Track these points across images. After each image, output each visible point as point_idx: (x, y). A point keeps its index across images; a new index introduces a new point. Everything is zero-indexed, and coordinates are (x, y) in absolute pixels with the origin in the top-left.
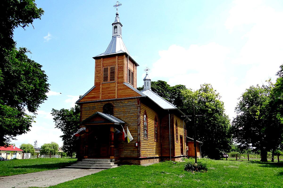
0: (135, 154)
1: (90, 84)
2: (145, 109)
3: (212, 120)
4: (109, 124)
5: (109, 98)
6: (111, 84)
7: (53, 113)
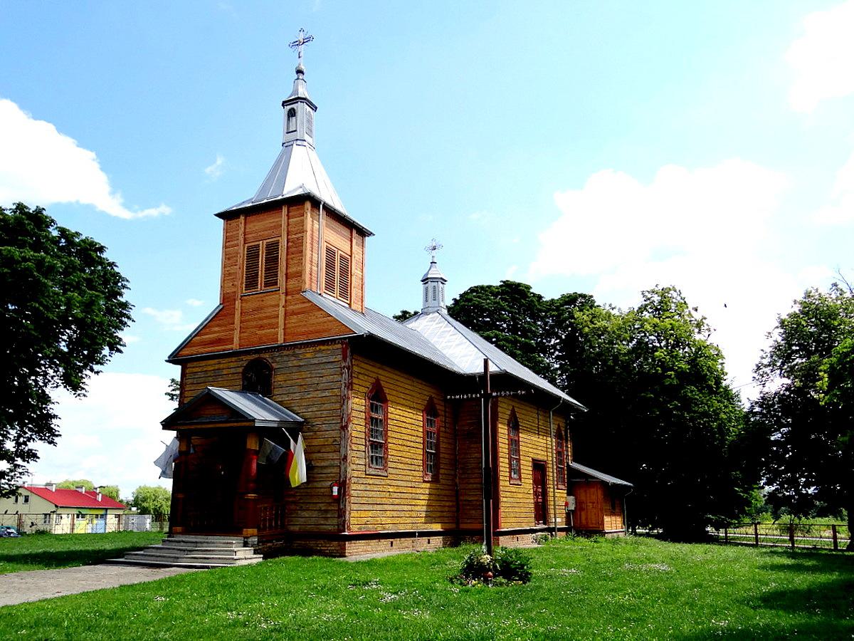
0: (330, 522)
1: (207, 302)
2: (375, 375)
3: (676, 408)
4: (239, 424)
5: (261, 342)
6: (267, 298)
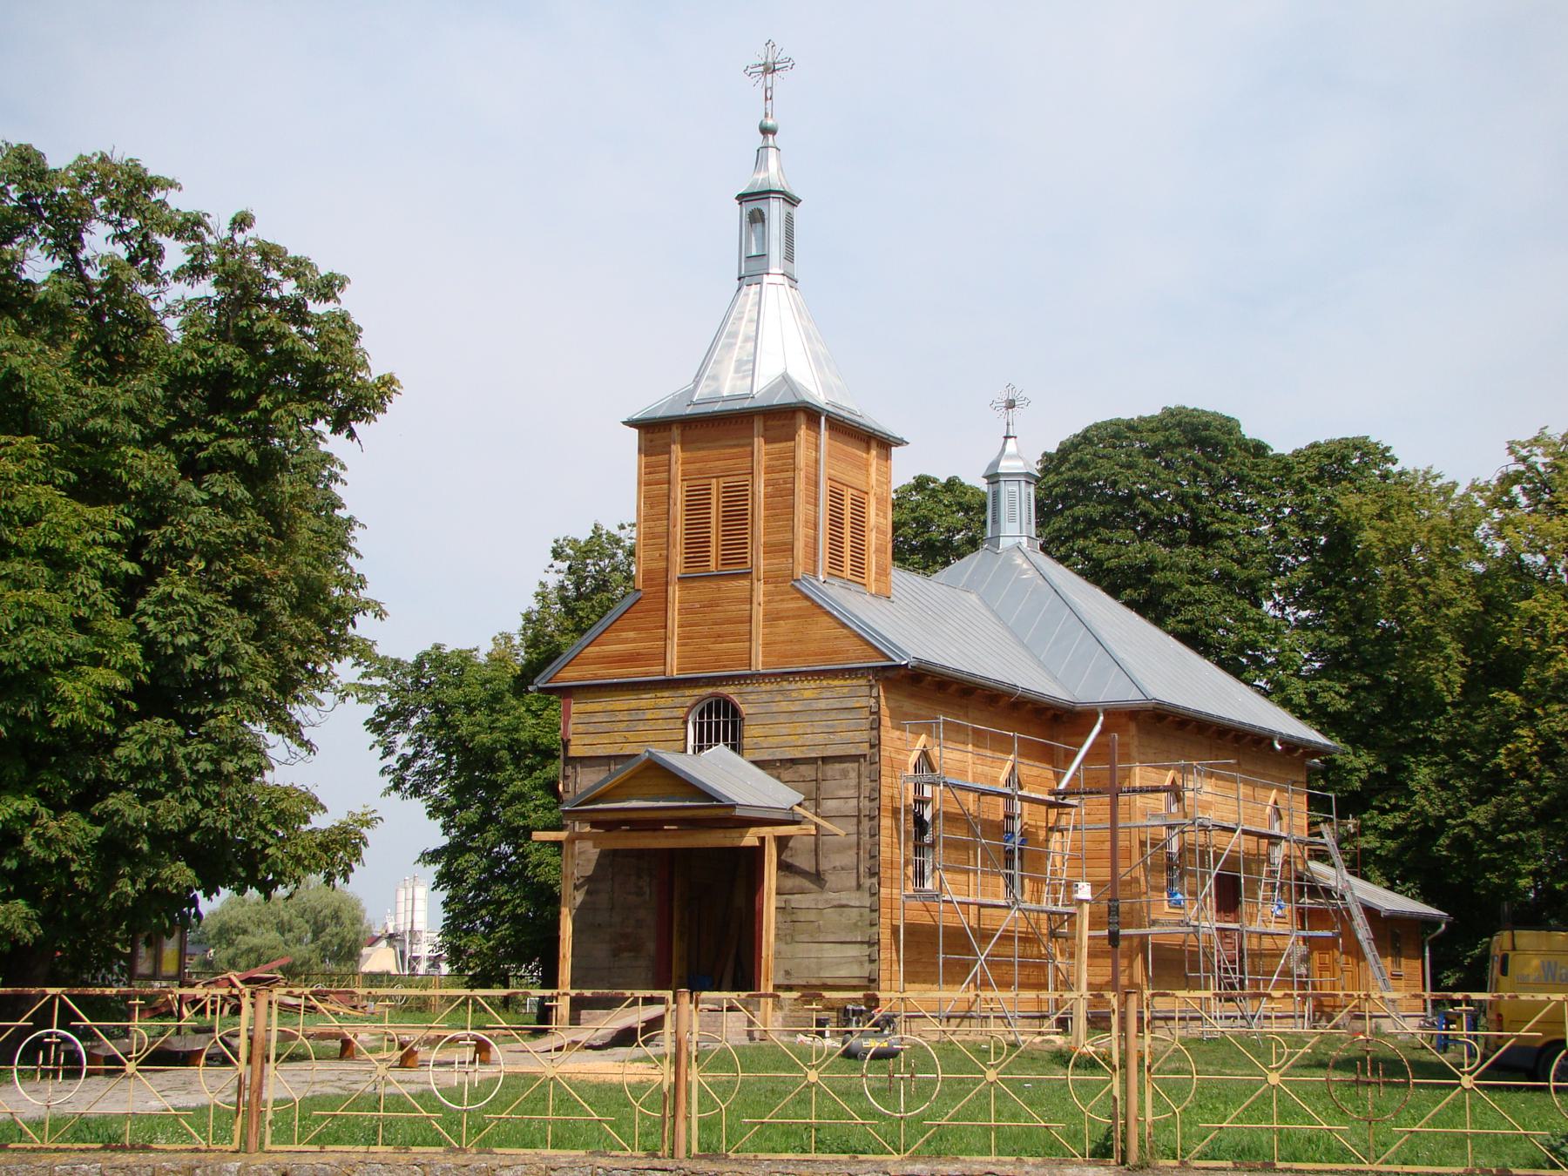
7: (366, 682)
